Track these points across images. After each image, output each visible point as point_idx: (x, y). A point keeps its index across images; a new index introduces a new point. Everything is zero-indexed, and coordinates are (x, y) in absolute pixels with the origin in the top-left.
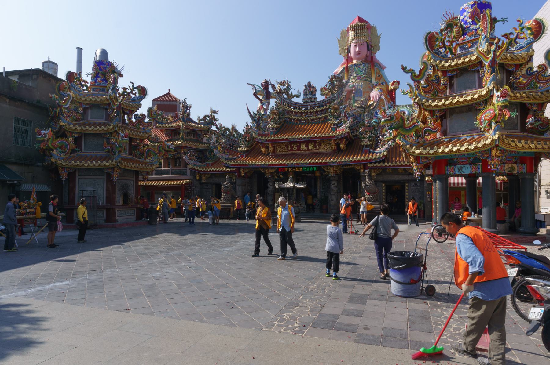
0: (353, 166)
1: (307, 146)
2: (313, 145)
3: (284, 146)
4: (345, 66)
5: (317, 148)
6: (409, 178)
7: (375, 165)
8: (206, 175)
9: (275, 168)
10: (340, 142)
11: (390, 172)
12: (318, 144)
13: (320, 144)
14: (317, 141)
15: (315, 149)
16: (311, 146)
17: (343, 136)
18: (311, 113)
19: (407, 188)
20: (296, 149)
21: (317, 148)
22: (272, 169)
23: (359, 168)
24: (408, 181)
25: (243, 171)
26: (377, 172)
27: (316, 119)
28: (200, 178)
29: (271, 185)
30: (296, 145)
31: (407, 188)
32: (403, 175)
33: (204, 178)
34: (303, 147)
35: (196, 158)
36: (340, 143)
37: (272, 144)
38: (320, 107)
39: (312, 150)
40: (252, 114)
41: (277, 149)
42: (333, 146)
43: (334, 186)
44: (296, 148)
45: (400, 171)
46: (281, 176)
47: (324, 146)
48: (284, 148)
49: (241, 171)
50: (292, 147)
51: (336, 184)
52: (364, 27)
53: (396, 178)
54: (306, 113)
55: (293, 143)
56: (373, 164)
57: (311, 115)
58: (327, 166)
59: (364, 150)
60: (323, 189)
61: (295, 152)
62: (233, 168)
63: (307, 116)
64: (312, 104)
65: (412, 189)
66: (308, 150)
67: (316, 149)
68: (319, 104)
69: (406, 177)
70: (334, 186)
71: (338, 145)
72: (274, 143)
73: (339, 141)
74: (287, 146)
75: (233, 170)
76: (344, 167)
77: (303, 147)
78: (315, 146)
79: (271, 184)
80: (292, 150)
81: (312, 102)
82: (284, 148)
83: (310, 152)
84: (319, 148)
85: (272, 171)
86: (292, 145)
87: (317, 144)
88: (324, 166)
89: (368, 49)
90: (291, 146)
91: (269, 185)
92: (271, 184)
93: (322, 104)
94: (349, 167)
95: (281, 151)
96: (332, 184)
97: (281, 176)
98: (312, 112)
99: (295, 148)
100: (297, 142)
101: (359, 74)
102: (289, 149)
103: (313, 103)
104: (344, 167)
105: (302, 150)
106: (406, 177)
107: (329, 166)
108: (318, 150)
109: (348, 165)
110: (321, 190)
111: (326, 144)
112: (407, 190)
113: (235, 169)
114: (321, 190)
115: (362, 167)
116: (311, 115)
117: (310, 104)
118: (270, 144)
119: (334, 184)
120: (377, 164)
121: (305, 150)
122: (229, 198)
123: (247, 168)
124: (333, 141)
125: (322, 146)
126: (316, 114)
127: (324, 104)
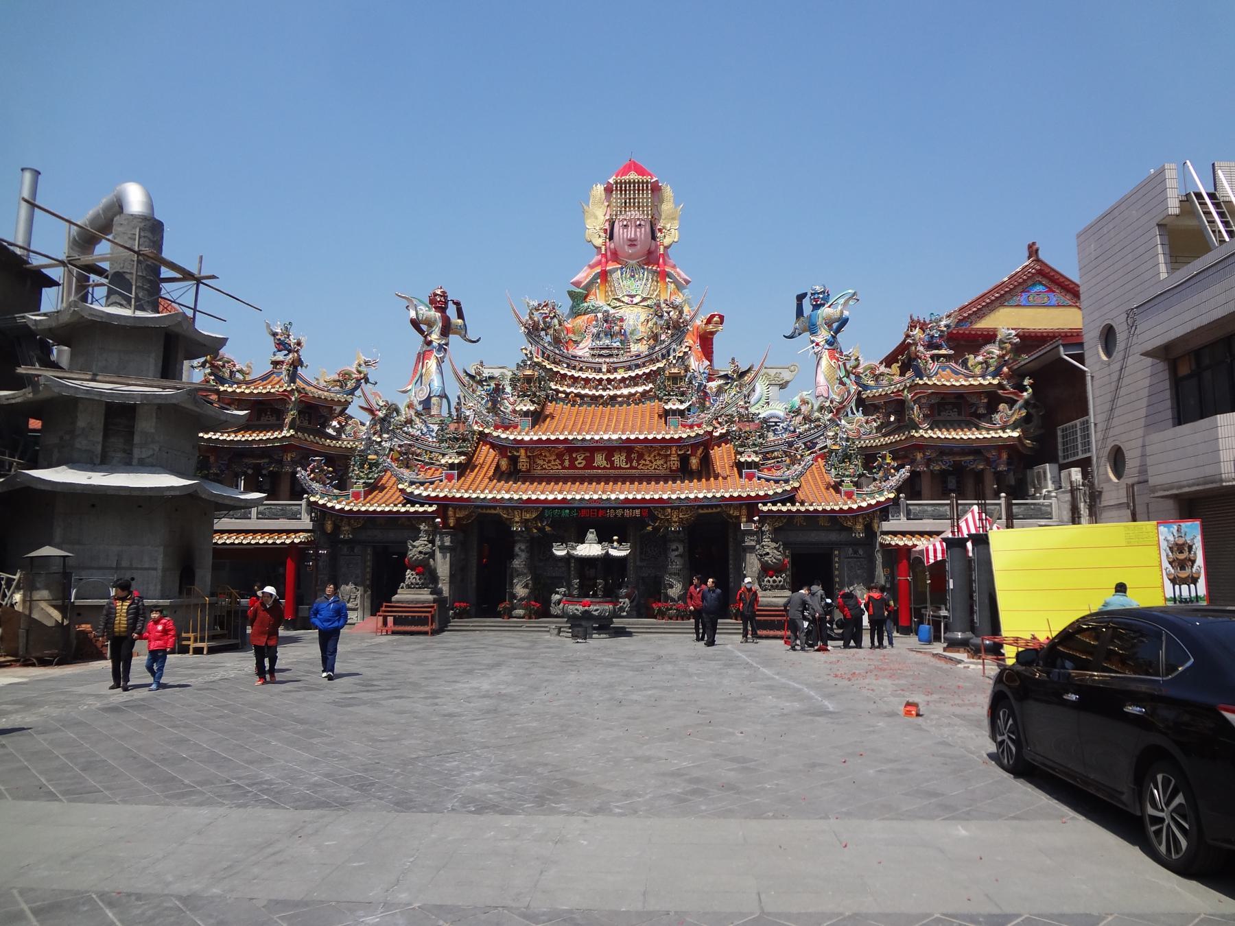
0: (719, 510)
1: (609, 458)
2: (623, 458)
3: (554, 457)
4: (598, 270)
5: (635, 464)
6: (843, 536)
7: (775, 508)
8: (352, 522)
9: (538, 508)
10: (689, 453)
11: (800, 524)
12: (636, 455)
13: (641, 456)
14: (634, 447)
15: (628, 466)
16: (619, 459)
17: (699, 440)
18: (609, 381)
19: (837, 559)
20: (581, 466)
21: (635, 464)
22: (528, 510)
23: (736, 513)
24: (839, 545)
25: (455, 513)
26: (777, 525)
27: (561, 392)
28: (337, 528)
29: (522, 551)
30: (583, 456)
31: (837, 559)
32: (828, 530)
33: (347, 528)
34: (600, 460)
35: (328, 478)
36: (690, 455)
37: (526, 449)
38: (629, 368)
39: (620, 468)
40: (462, 375)
41: (534, 462)
42: (674, 462)
43: (676, 553)
44: (584, 462)
45: (822, 523)
46: (548, 529)
47: (651, 461)
48: (555, 460)
49: (450, 513)
50: (572, 460)
51: (681, 549)
52: (647, 187)
53: (815, 537)
54: (598, 380)
55: (577, 449)
56: (769, 507)
57: (609, 386)
58: (664, 508)
59: (746, 473)
60: (642, 560)
61: (581, 472)
62: (431, 505)
63: (600, 387)
64: (611, 360)
65: (849, 562)
66: (613, 467)
67: (632, 468)
68: (629, 363)
69: (834, 537)
70: (676, 553)
71: (684, 460)
72: (532, 448)
73: (688, 450)
74: (560, 456)
75: (430, 509)
76: (701, 511)
77: (600, 460)
78: (629, 460)
79: (523, 547)
80: (572, 466)
81: (611, 356)
82: (555, 460)
83: (617, 472)
84: (639, 464)
85: (528, 516)
86: (574, 456)
87: (633, 456)
88: (655, 507)
90: (571, 456)
91: (517, 549)
92: (523, 547)
93: (636, 362)
94: (710, 511)
95: (545, 469)
96: (673, 550)
97: (548, 529)
98: (613, 380)
99: (580, 461)
100: (585, 449)
101: (633, 290)
102: (567, 463)
103: (615, 360)
104: (701, 511)
105: (599, 468)
106: (834, 537)
107: (669, 507)
108: (636, 468)
109: (707, 507)
110: (638, 563)
111: (655, 456)
112: (837, 565)
113: (434, 508)
114: (638, 563)
115: (744, 512)
116: (609, 386)
117: (607, 360)
118: (522, 452)
119: (677, 549)
120: (779, 507)
121: (605, 468)
122: (425, 579)
123: (465, 507)
124: (674, 449)
125: (645, 460)
126: (622, 385)
127: (639, 362)
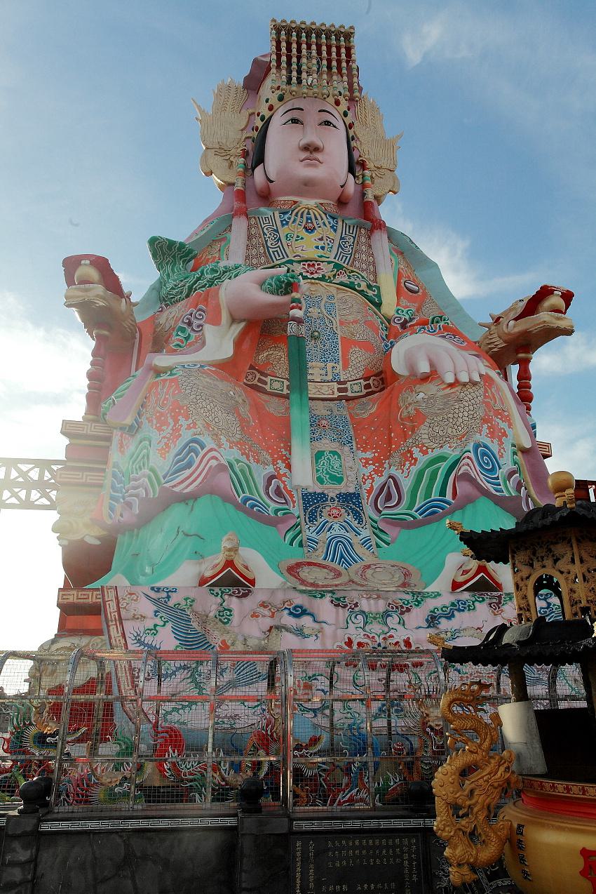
89: (351, 170)
